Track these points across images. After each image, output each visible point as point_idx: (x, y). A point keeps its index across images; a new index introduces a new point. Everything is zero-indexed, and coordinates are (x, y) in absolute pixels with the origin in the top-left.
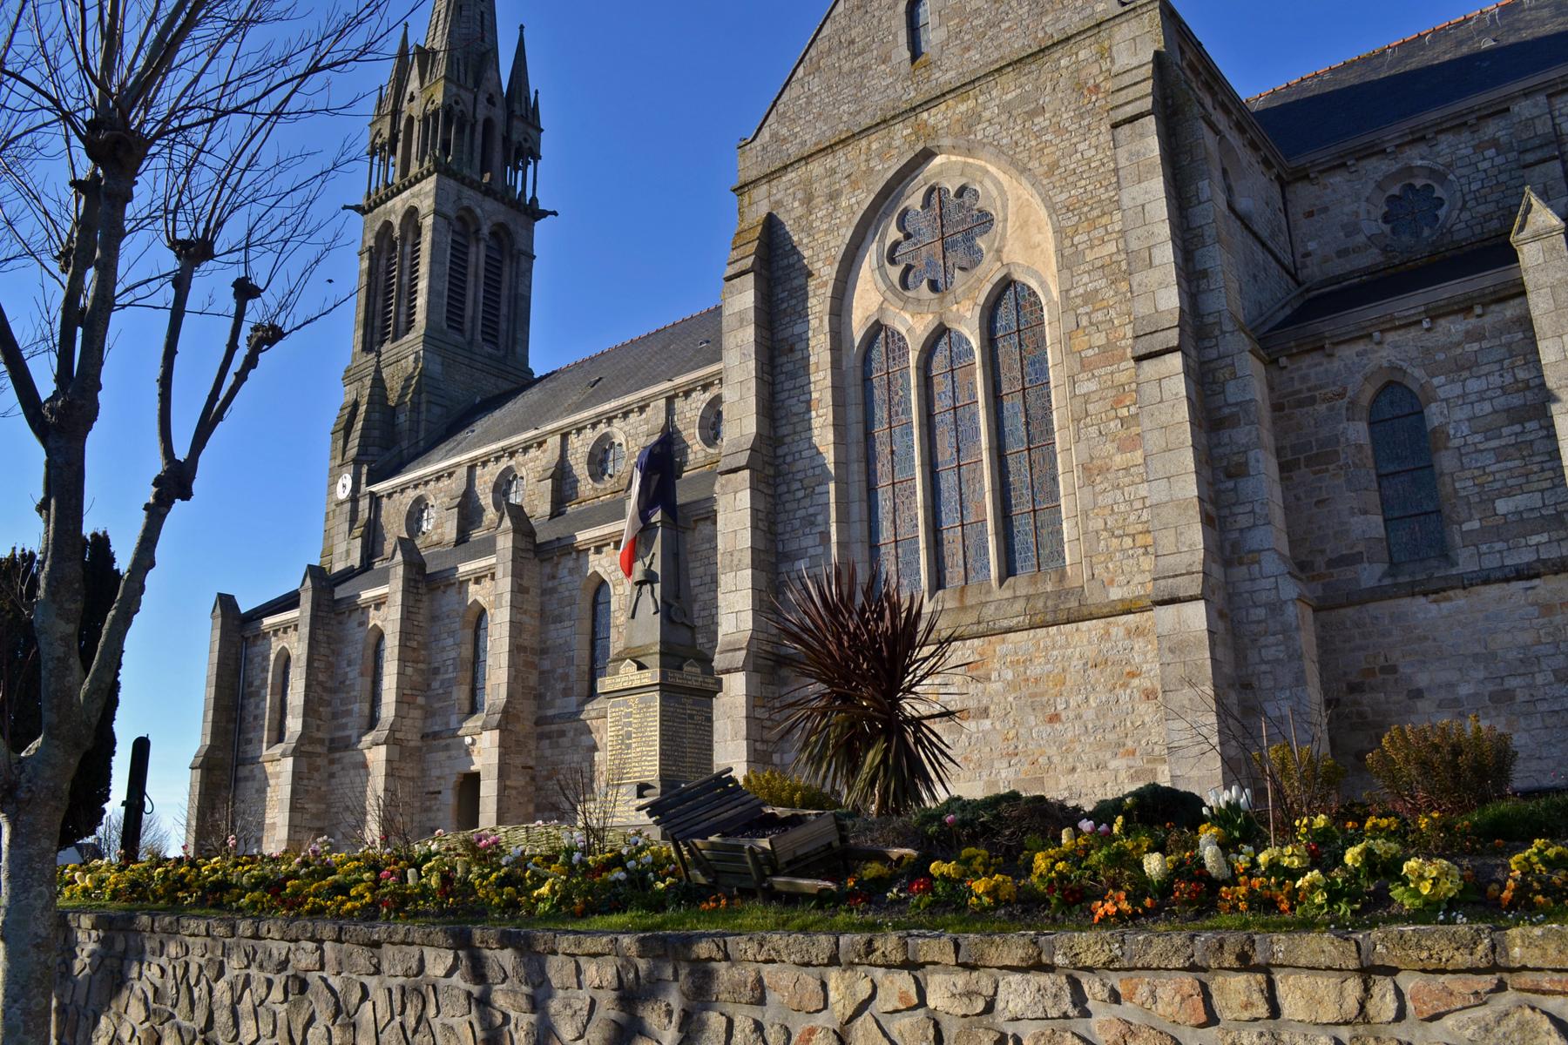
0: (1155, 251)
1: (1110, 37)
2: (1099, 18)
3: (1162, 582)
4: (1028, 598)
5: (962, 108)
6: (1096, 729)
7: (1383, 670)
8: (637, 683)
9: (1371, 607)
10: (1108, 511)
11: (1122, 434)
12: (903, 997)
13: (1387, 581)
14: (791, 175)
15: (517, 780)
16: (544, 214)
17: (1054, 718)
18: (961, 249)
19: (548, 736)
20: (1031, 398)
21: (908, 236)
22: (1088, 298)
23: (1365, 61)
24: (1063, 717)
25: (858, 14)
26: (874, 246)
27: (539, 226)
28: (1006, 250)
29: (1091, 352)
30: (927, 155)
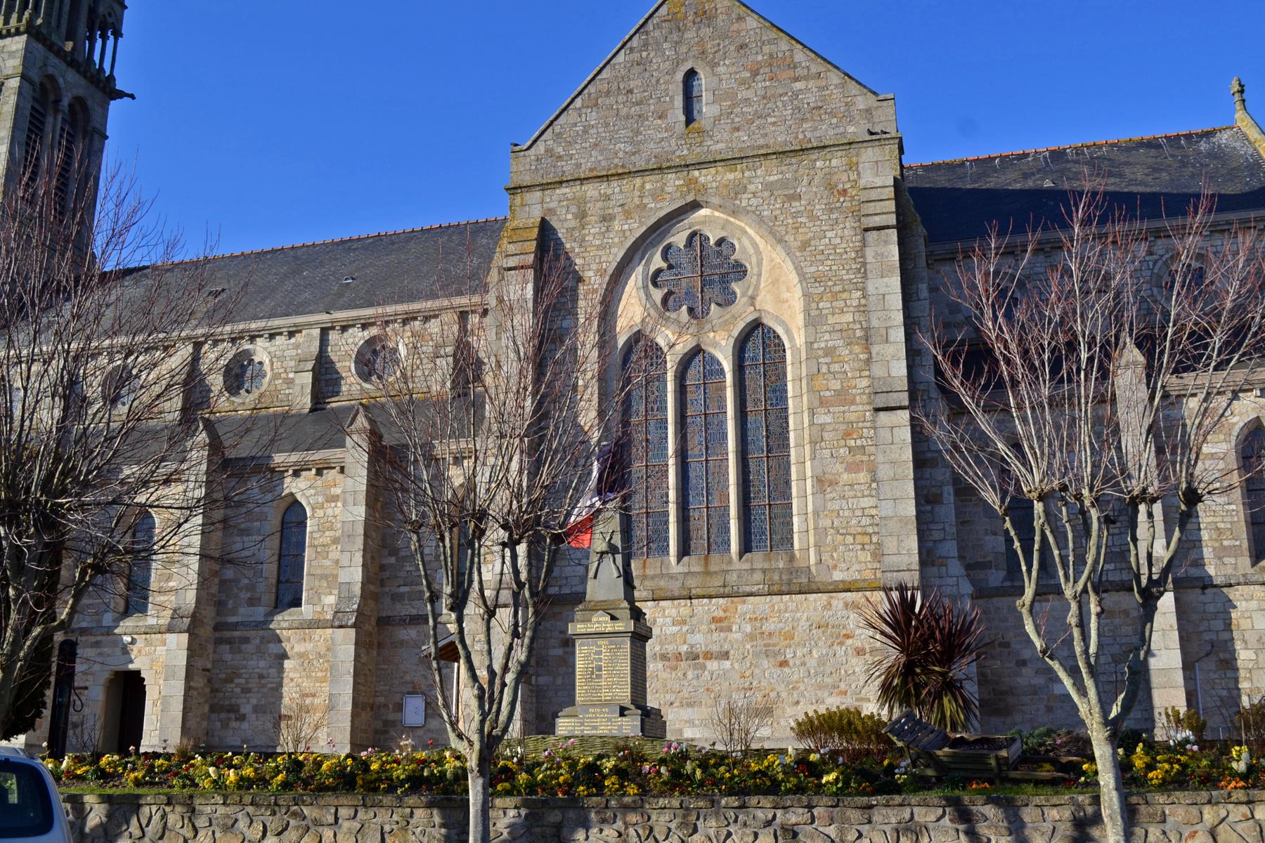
0: (890, 331)
1: (858, 155)
2: (850, 138)
3: (889, 575)
4: (764, 571)
5: (730, 176)
6: (816, 674)
7: (1001, 645)
8: (609, 629)
9: (995, 600)
10: (835, 514)
11: (850, 459)
12: (1244, 815)
13: (1007, 584)
14: (565, 190)
15: (199, 682)
16: (121, 95)
17: (784, 664)
18: (717, 288)
19: (229, 641)
20: (772, 418)
21: (670, 267)
22: (829, 352)
23: (950, 167)
24: (791, 663)
25: (636, 70)
26: (640, 269)
27: (114, 105)
28: (759, 298)
29: (828, 394)
30: (695, 206)
